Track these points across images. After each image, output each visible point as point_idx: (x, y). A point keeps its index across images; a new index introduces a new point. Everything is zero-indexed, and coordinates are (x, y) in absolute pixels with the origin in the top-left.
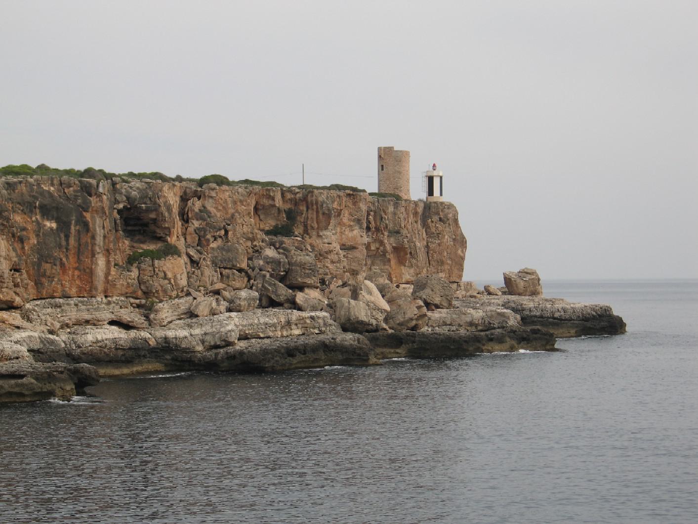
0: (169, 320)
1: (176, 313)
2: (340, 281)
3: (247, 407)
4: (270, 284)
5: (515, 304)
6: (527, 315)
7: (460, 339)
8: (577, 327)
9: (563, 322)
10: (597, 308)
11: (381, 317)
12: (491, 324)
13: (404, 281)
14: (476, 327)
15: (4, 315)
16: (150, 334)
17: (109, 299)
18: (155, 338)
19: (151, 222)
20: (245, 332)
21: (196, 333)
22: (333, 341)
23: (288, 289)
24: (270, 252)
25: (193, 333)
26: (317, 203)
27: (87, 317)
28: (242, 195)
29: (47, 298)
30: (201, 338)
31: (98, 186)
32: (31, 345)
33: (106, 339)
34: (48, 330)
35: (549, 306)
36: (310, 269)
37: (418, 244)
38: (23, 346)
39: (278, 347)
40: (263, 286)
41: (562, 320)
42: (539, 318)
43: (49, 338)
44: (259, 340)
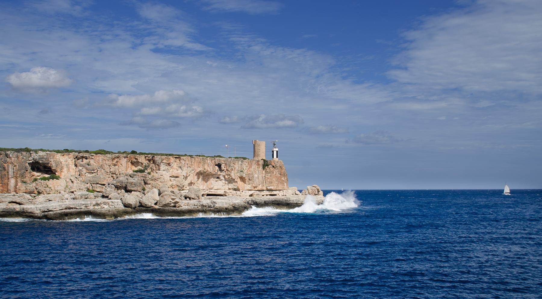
1: (45, 199)
3: (443, 254)
36: (134, 185)
38: (480, 229)
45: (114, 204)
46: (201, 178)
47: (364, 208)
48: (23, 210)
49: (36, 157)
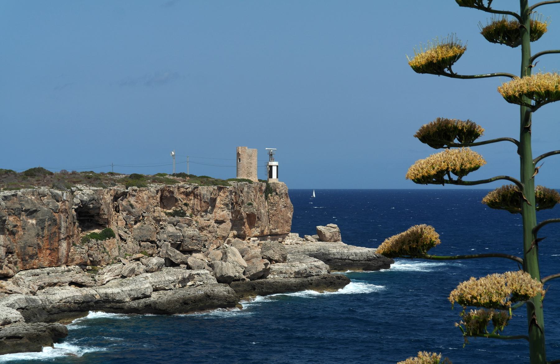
0: (107, 280)
1: (113, 275)
2: (215, 245)
4: (171, 252)
9: (355, 262)
11: (242, 271)
12: (310, 273)
13: (253, 235)
14: (301, 275)
15: (4, 283)
16: (96, 291)
17: (69, 267)
18: (99, 294)
19: (96, 215)
20: (156, 287)
21: (125, 290)
22: (212, 292)
24: (171, 229)
25: (123, 290)
26: (200, 195)
27: (55, 281)
29: (29, 269)
30: (129, 292)
31: (63, 195)
32: (21, 305)
33: (68, 297)
34: (31, 291)
35: (346, 251)
37: (263, 211)
39: (178, 298)
40: (167, 252)
41: (354, 261)
43: (32, 299)
44: (165, 292)
47: (409, 267)
49: (85, 197)
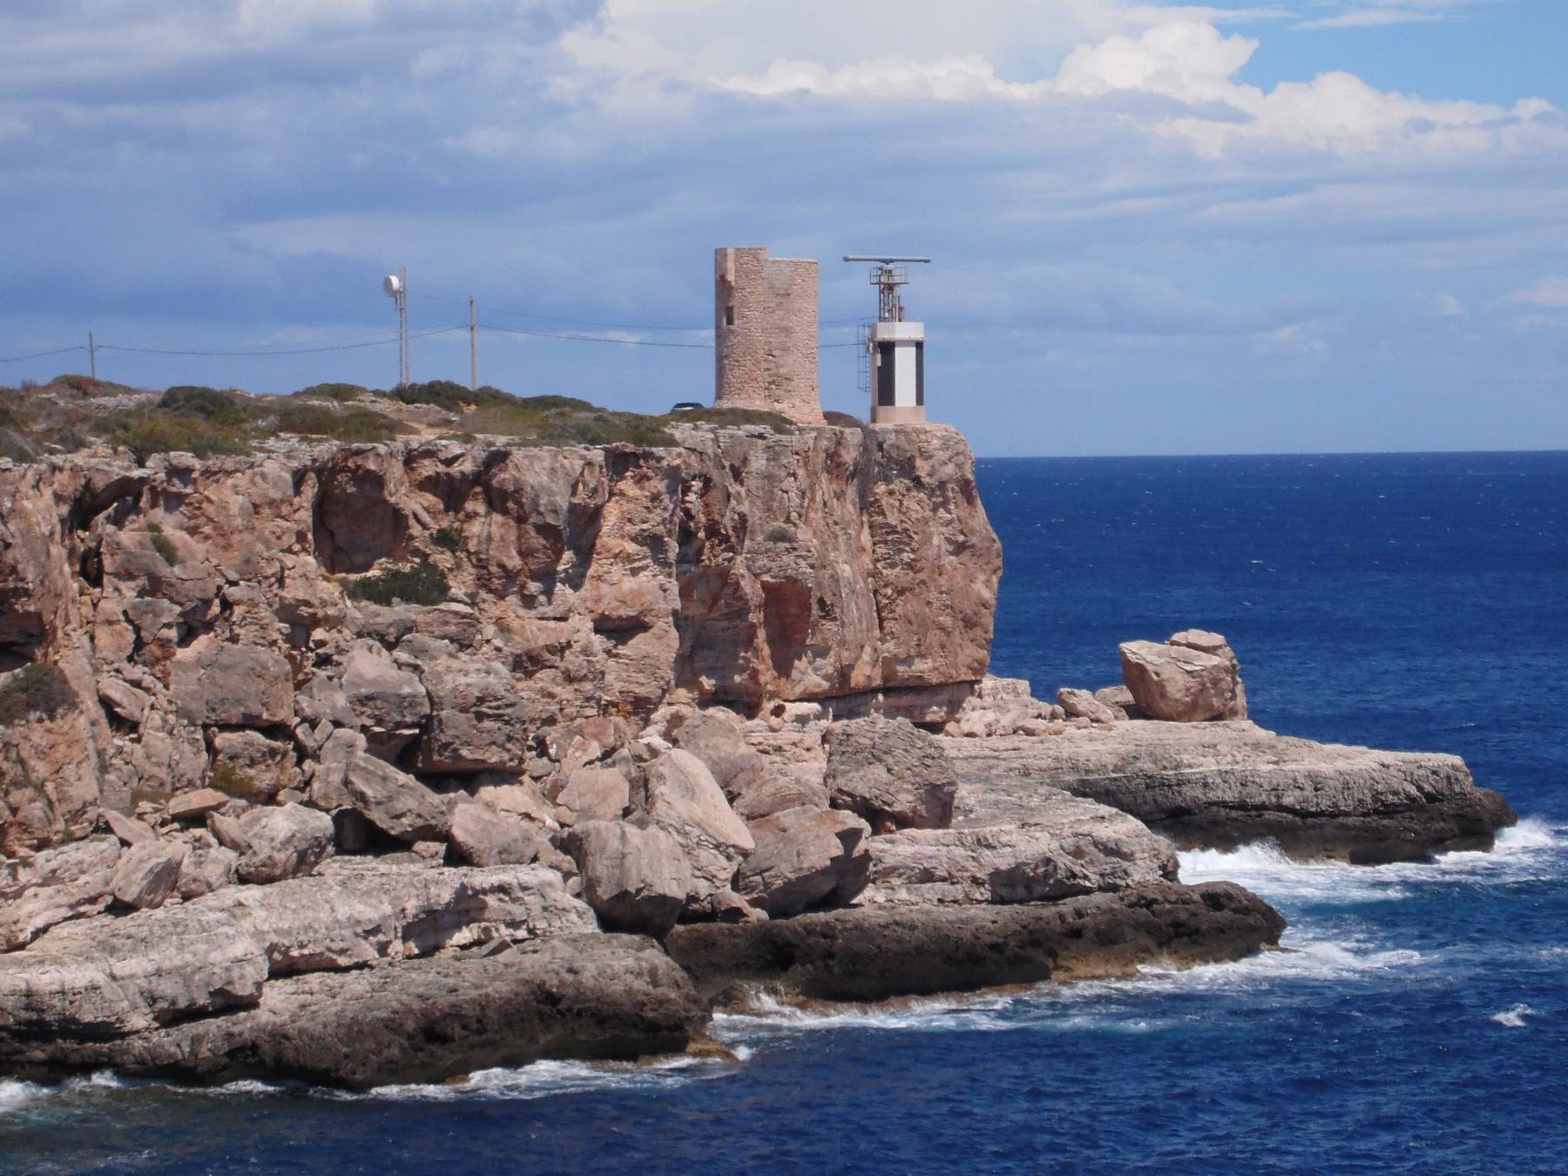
0: (39, 922)
4: (368, 774)
5: (1155, 762)
6: (1194, 799)
7: (977, 938)
8: (1355, 839)
9: (1310, 820)
10: (1422, 772)
12: (1074, 876)
23: (427, 791)
28: (275, 485)
39: (395, 1012)
42: (1232, 808)
44: (333, 979)
45: (518, 911)
46: (1369, 800)
48: (28, 1008)
